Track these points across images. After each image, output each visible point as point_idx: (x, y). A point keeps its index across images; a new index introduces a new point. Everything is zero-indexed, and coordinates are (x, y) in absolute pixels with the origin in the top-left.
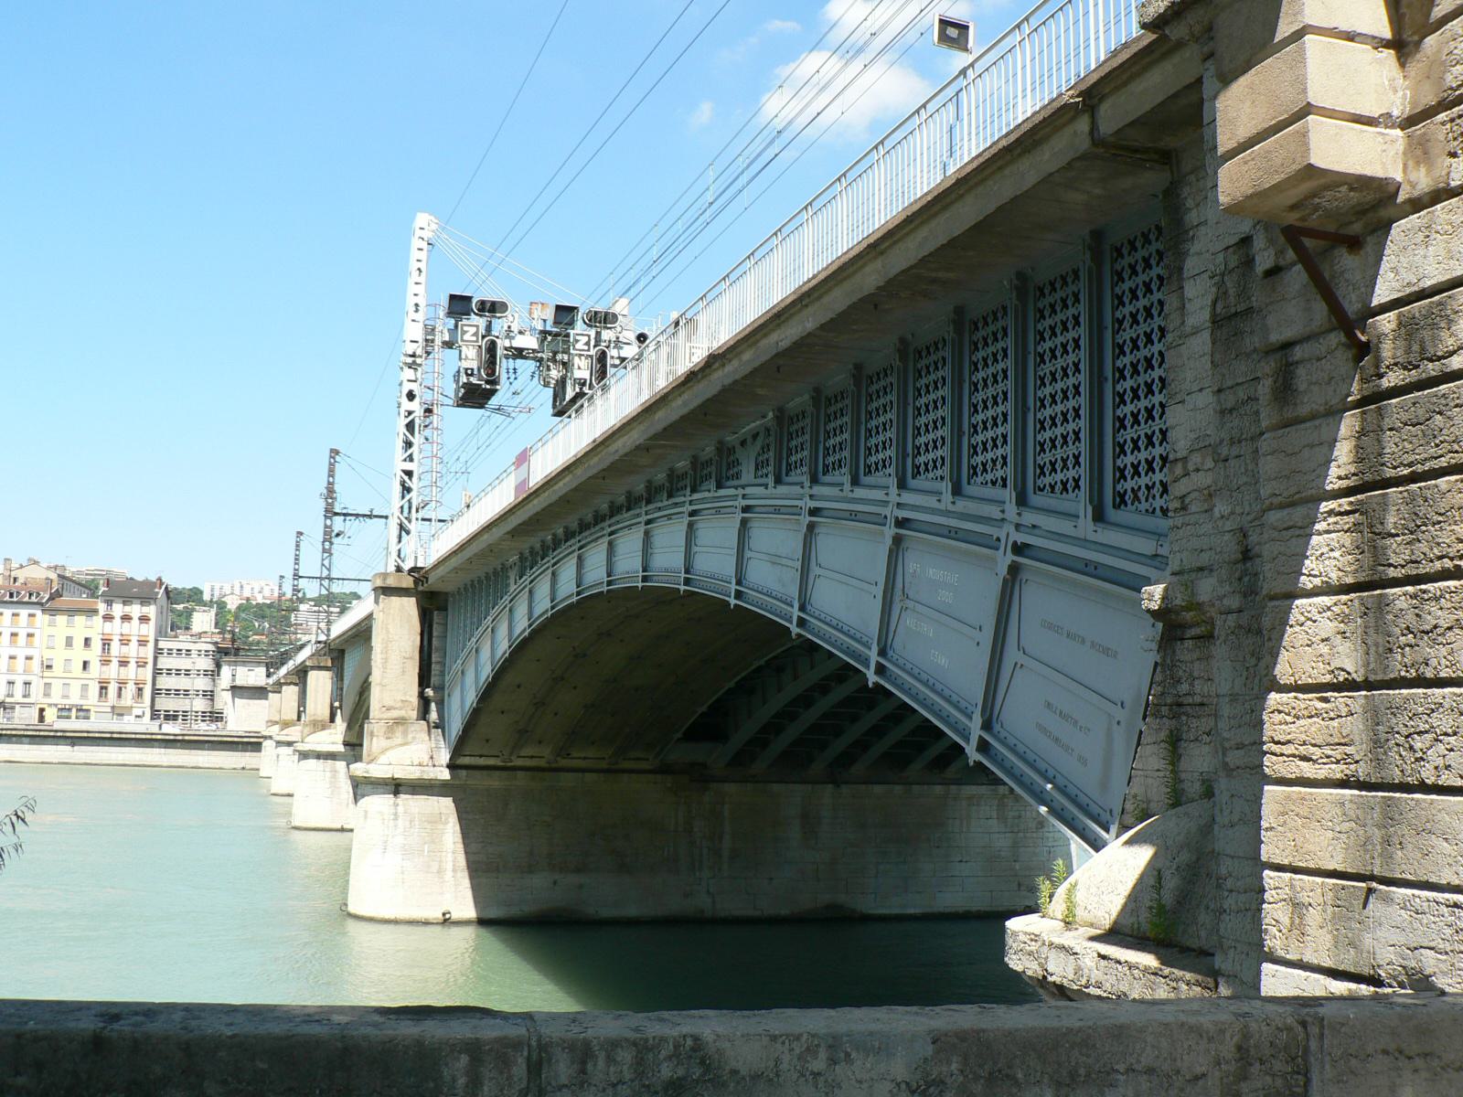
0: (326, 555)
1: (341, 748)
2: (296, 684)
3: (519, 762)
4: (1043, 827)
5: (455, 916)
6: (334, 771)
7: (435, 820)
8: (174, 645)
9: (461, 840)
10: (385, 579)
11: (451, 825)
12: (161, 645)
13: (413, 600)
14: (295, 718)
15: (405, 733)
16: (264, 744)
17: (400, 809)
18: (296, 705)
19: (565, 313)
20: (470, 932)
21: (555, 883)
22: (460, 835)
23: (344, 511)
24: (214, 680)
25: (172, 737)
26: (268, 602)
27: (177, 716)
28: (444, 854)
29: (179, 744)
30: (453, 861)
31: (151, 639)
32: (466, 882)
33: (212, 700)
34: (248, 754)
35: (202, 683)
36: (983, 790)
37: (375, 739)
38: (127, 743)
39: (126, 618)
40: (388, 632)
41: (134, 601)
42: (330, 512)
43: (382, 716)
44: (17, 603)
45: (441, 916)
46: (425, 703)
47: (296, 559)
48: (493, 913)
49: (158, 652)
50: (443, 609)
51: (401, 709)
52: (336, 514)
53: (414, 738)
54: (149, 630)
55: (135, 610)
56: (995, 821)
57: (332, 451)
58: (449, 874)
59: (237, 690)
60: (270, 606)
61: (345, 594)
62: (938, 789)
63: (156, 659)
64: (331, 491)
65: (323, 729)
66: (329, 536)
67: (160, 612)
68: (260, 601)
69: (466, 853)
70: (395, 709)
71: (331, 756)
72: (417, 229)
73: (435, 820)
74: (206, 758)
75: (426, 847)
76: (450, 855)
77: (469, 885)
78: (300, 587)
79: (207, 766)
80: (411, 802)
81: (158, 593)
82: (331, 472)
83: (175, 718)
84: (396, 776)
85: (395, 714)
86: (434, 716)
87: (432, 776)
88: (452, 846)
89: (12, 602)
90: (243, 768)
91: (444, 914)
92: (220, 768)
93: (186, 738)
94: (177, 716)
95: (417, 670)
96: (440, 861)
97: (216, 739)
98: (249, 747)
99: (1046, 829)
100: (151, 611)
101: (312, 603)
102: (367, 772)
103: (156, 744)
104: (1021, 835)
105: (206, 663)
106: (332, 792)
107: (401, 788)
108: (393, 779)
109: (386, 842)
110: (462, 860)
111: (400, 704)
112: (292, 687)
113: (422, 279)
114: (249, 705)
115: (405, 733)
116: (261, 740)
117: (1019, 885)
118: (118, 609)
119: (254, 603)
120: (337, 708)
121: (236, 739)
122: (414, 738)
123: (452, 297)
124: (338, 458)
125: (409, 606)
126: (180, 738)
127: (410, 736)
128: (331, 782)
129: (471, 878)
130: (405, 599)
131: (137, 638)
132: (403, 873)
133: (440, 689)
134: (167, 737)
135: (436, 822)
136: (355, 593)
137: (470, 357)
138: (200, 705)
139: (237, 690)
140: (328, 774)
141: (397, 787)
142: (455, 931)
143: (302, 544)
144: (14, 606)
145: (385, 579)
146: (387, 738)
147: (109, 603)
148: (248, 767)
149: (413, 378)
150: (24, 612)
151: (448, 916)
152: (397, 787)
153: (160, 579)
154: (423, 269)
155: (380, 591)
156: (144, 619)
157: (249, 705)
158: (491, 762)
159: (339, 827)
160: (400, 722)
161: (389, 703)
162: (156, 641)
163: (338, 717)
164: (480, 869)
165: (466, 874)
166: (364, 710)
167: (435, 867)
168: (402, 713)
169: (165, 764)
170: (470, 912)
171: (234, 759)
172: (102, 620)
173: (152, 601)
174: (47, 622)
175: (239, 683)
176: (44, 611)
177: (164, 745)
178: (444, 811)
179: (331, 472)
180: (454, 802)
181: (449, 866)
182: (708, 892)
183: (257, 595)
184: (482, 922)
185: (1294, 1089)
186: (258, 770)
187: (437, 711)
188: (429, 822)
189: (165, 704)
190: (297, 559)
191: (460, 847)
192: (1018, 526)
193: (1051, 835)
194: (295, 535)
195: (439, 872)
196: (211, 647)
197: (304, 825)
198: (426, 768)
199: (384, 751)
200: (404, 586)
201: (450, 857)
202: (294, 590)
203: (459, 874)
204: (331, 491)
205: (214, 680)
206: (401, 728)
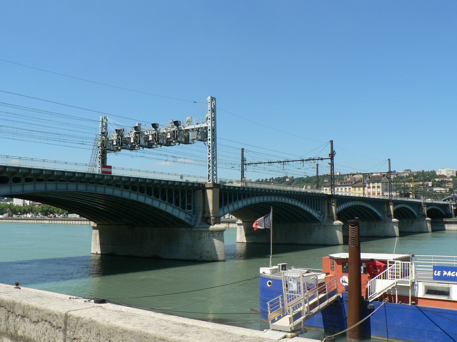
4: (200, 239)
31: (381, 192)
32: (100, 246)
36: (184, 229)
39: (374, 187)
41: (375, 182)
44: (345, 185)
54: (380, 190)
55: (376, 185)
56: (189, 237)
58: (98, 245)
89: (344, 185)
99: (201, 240)
100: (380, 184)
110: (99, 243)
118: (371, 185)
123: (332, 141)
129: (100, 246)
131: (372, 193)
144: (345, 186)
147: (369, 183)
150: (348, 188)
156: (378, 187)
162: (383, 193)
172: (367, 188)
174: (353, 190)
176: (352, 187)
181: (98, 243)
185: (124, 341)
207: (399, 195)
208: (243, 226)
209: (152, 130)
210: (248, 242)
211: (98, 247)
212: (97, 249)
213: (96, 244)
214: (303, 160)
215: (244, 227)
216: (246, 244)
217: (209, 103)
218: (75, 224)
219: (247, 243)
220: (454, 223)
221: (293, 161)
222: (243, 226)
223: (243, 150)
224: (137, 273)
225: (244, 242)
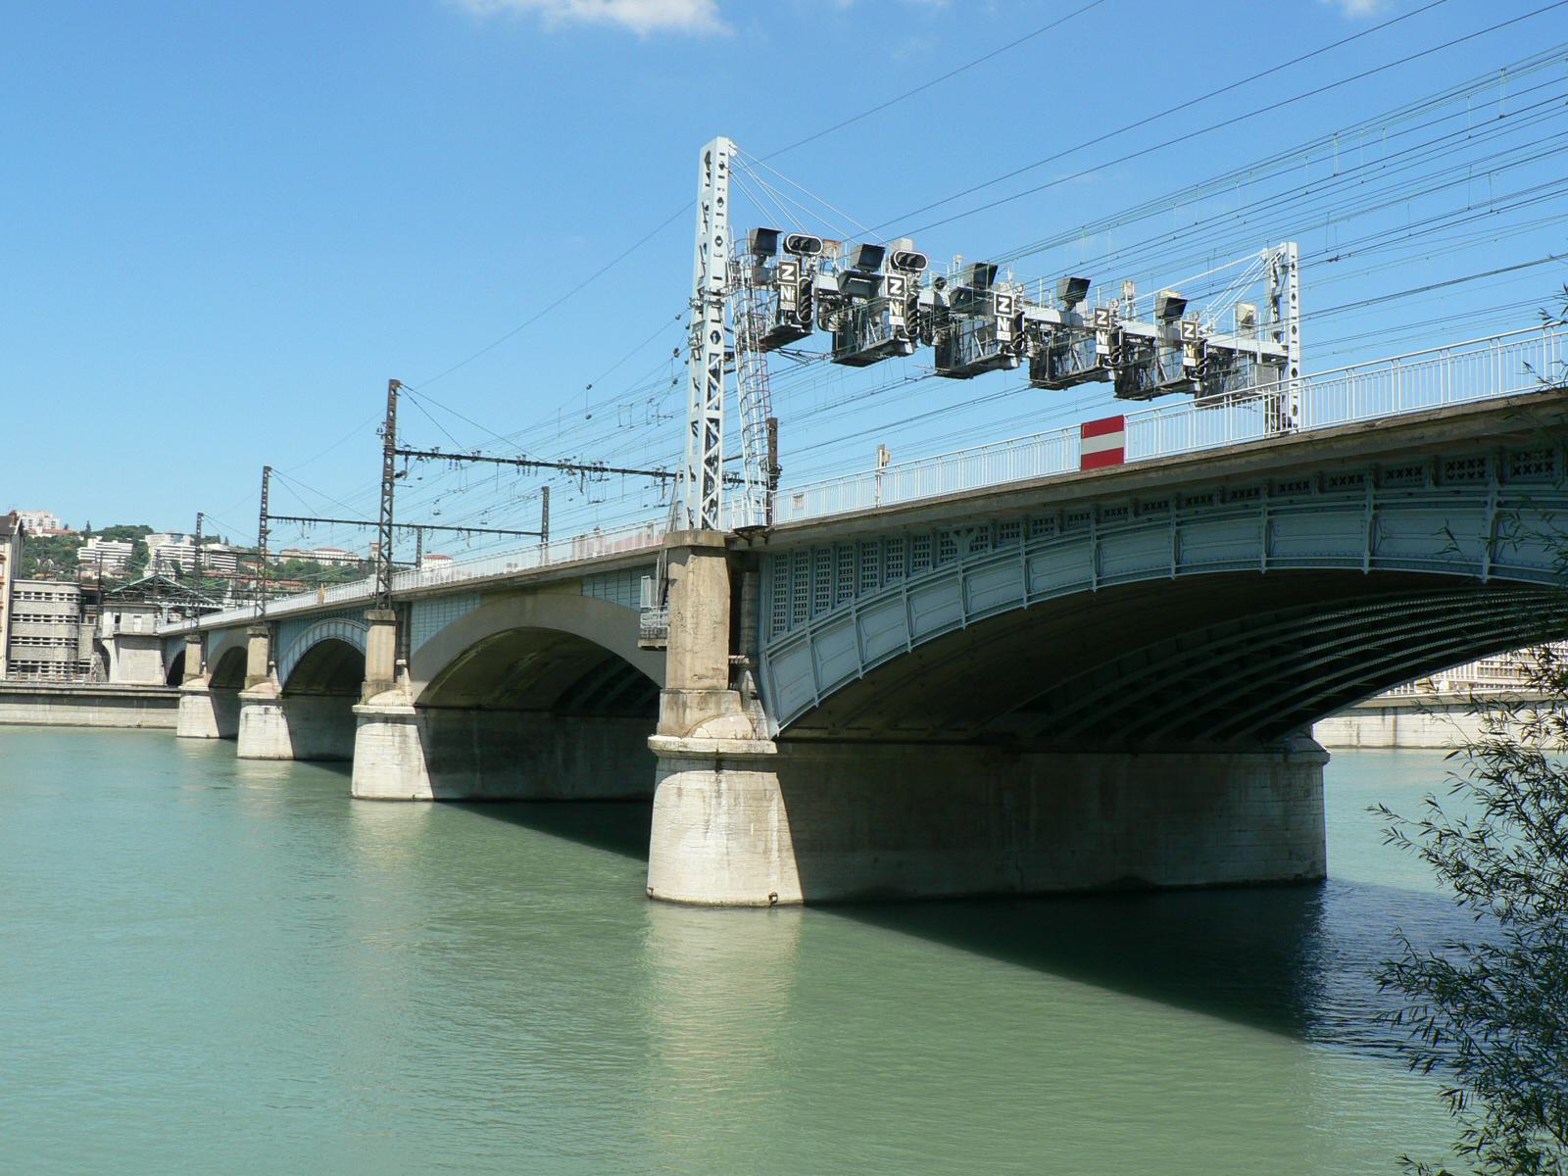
0: (387, 497)
1: (412, 711)
2: (264, 636)
3: (844, 734)
5: (782, 898)
6: (404, 736)
7: (761, 797)
8: (33, 588)
9: (786, 818)
10: (696, 537)
11: (775, 801)
12: (18, 587)
13: (723, 560)
14: (264, 673)
15: (718, 704)
16: (181, 700)
17: (724, 786)
18: (266, 658)
19: (872, 255)
20: (794, 917)
21: (876, 860)
22: (785, 813)
23: (407, 449)
24: (78, 627)
25: (58, 692)
26: (50, 536)
27: (37, 667)
28: (769, 833)
29: (65, 700)
30: (779, 841)
32: (792, 863)
33: (76, 649)
34: (144, 710)
35: (63, 631)
37: (688, 710)
38: (6, 698)
40: (699, 595)
42: (390, 451)
43: (692, 686)
45: (768, 899)
46: (735, 672)
47: (263, 498)
48: (818, 894)
49: (14, 595)
50: (755, 570)
51: (712, 678)
52: (398, 452)
53: (727, 709)
57: (392, 382)
58: (775, 854)
59: (121, 639)
60: (53, 540)
61: (134, 527)
62: (1223, 757)
63: (11, 603)
64: (391, 423)
65: (387, 690)
66: (390, 477)
67: (14, 551)
68: (40, 534)
69: (791, 831)
70: (707, 677)
71: (401, 719)
72: (718, 155)
73: (761, 797)
74: (97, 715)
75: (752, 825)
76: (775, 834)
77: (795, 866)
78: (268, 528)
79: (98, 723)
80: (735, 778)
81: (13, 529)
82: (392, 406)
83: (34, 669)
84: (721, 751)
85: (707, 683)
86: (749, 684)
87: (759, 750)
88: (777, 824)
90: (139, 726)
91: (771, 897)
92: (113, 726)
93: (75, 693)
94: (37, 667)
95: (728, 637)
96: (766, 841)
97: (108, 693)
98: (145, 703)
101: (100, 538)
102: (685, 747)
103: (40, 699)
104: (1292, 803)
105: (66, 608)
106: (402, 758)
107: (723, 764)
108: (717, 753)
109: (708, 821)
110: (787, 837)
111: (710, 673)
112: (261, 639)
113: (724, 210)
114: (135, 655)
115: (718, 704)
116: (179, 695)
117: (1290, 853)
119: (33, 537)
120: (272, 666)
121: (131, 694)
122: (727, 709)
124: (399, 391)
125: (718, 566)
126: (68, 693)
127: (723, 707)
128: (401, 748)
129: (797, 857)
130: (715, 559)
132: (728, 854)
133: (754, 656)
134: (53, 692)
135: (761, 800)
136: (146, 527)
137: (789, 298)
138: (61, 654)
139: (121, 639)
140: (397, 739)
141: (718, 762)
142: (781, 913)
143: (270, 480)
145: (696, 537)
146: (701, 710)
148: (144, 724)
149: (718, 319)
151: (774, 899)
152: (718, 762)
153: (13, 513)
154: (725, 199)
155: (689, 550)
157: (135, 655)
158: (816, 734)
159: (410, 796)
160: (712, 691)
161: (700, 670)
162: (12, 583)
163: (205, 673)
164: (807, 846)
165: (792, 853)
166: (1310, 709)
167: (761, 849)
168: (714, 682)
169: (51, 722)
170: (793, 892)
171: (128, 716)
173: (7, 539)
175: (124, 629)
177: (47, 701)
178: (769, 787)
179: (392, 406)
180: (778, 777)
181: (775, 846)
182: (1017, 867)
183: (35, 527)
184: (808, 904)
186: (176, 728)
187: (754, 681)
188: (756, 799)
189: (23, 654)
190: (264, 498)
191: (785, 825)
192: (1499, 493)
193: (1315, 802)
194: (262, 470)
195: (765, 853)
196: (74, 590)
197: (371, 795)
198: (752, 742)
199: (699, 723)
200: (715, 544)
201: (775, 837)
202: (261, 531)
203: (784, 854)
204: (391, 423)
205: (78, 627)
206: (714, 698)
207: (77, 595)
208: (414, 727)
209: (1108, 311)
210: (440, 796)
211: (783, 865)
212: (774, 878)
213: (767, 851)
214: (664, 475)
215: (419, 729)
216: (427, 806)
217: (720, 200)
218: (1395, 747)
219: (436, 800)
220: (97, 701)
221: (498, 461)
222: (414, 727)
223: (394, 385)
224: (1092, 989)
225: (421, 796)
